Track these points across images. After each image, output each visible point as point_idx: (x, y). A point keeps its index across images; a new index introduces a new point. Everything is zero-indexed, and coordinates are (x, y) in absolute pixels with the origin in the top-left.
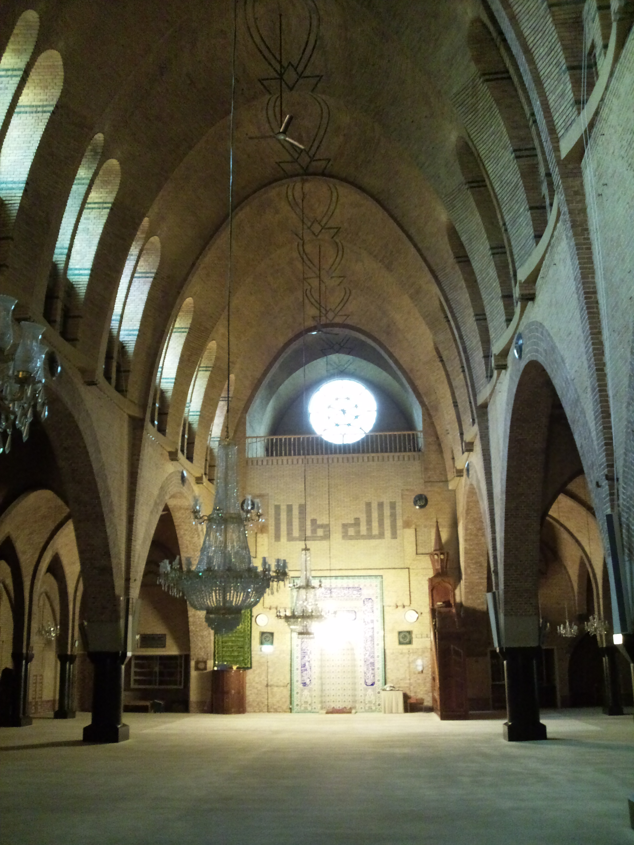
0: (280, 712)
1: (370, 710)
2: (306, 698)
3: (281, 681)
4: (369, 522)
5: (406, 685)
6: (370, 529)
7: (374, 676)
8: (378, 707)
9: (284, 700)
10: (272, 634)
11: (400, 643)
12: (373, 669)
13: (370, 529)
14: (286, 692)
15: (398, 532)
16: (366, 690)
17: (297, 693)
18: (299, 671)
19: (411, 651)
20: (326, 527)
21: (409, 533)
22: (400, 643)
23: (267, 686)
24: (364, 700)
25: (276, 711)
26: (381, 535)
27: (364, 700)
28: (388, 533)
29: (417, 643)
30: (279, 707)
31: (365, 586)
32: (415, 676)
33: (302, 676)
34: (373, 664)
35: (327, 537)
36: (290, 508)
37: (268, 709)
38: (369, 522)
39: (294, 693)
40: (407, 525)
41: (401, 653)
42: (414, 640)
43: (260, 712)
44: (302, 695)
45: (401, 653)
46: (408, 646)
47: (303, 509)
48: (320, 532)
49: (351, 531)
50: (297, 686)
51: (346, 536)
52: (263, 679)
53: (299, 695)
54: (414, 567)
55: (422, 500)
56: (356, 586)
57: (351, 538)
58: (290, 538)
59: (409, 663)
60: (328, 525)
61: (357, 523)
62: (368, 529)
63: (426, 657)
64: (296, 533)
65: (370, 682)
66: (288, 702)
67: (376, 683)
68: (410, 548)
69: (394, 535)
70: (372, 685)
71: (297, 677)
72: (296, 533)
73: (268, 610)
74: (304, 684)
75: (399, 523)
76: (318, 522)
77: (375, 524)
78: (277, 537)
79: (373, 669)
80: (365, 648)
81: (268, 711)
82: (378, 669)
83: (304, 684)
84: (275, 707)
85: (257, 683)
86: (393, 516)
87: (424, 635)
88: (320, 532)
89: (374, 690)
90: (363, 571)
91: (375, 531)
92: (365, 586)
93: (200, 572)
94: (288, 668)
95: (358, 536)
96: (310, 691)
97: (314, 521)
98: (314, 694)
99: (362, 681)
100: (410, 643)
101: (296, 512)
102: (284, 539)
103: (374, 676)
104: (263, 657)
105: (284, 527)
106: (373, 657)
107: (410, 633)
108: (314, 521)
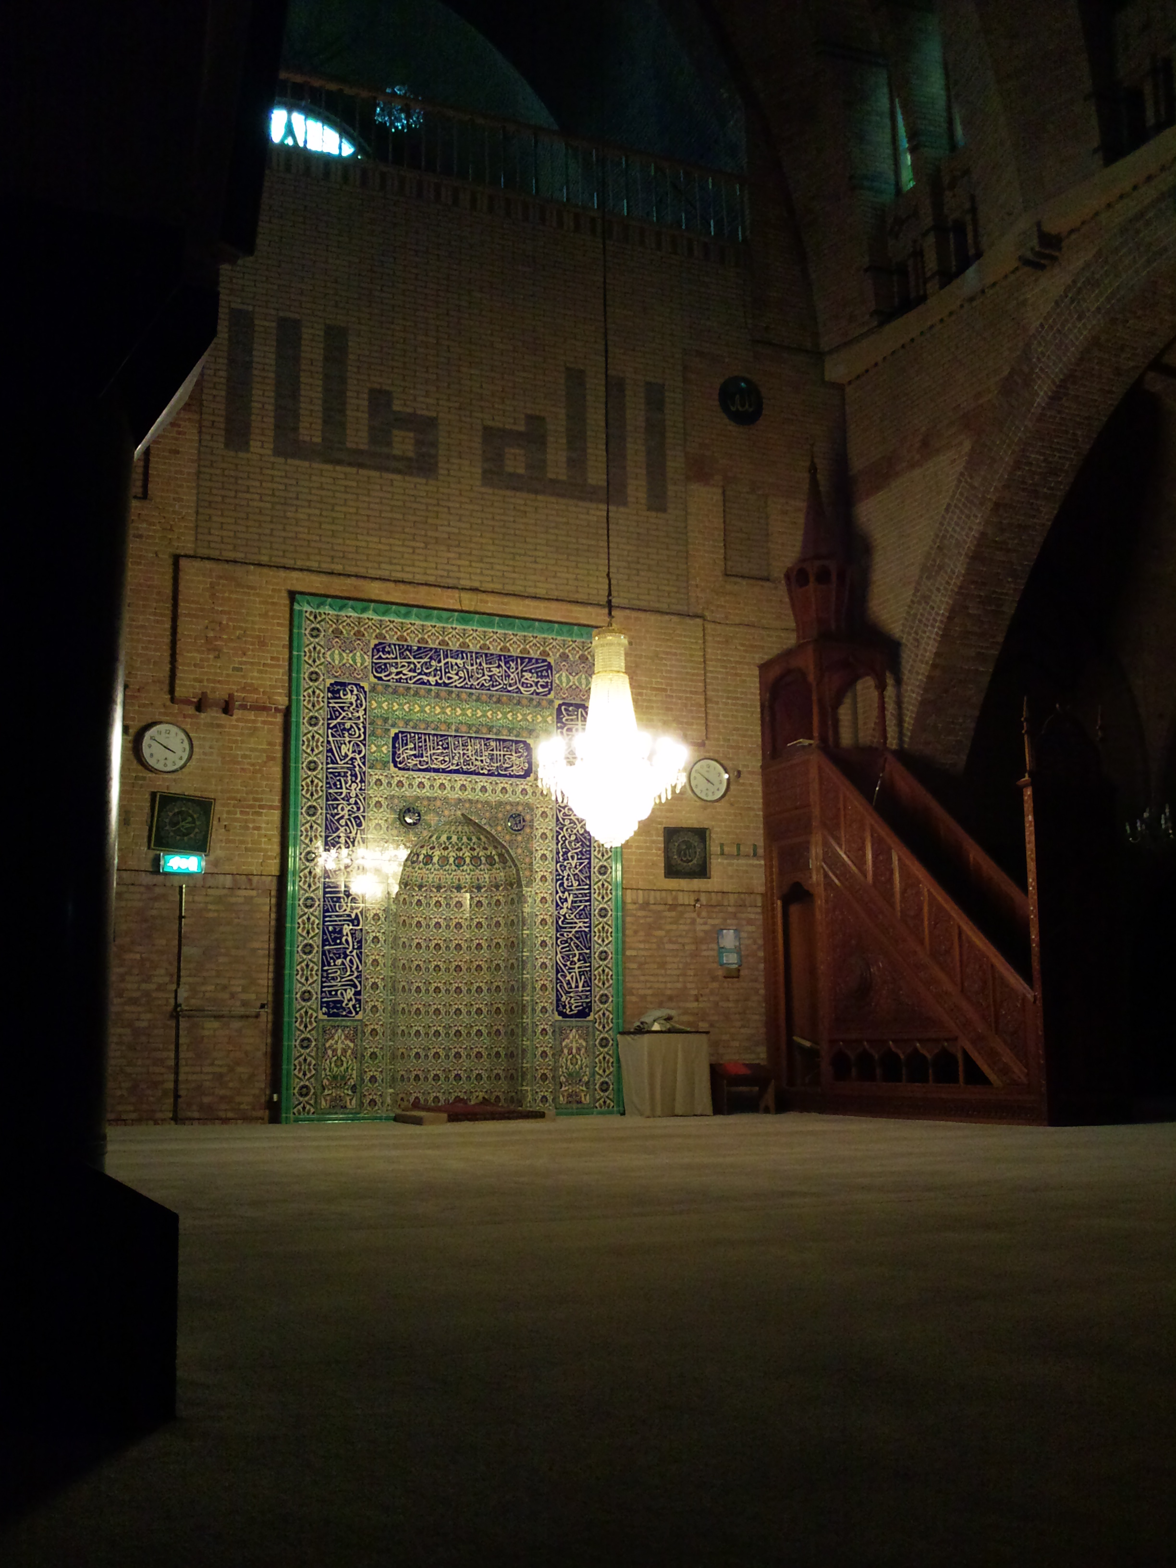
0: (225, 1121)
1: (575, 1107)
2: (339, 1062)
3: (233, 996)
4: (576, 439)
5: (482, 1067)
6: (577, 463)
7: (588, 984)
8: (599, 1094)
9: (243, 1070)
10: (204, 806)
11: (671, 871)
12: (585, 958)
13: (577, 463)
14: (255, 1041)
15: (671, 489)
16: (559, 1033)
17: (305, 1043)
18: (316, 956)
19: (703, 899)
20: (424, 427)
21: (704, 500)
22: (671, 871)
23: (176, 1013)
24: (554, 1069)
25: (210, 1116)
26: (613, 493)
27: (554, 1069)
28: (637, 488)
29: (723, 874)
30: (222, 1098)
31: (564, 657)
32: (715, 985)
33: (326, 977)
34: (584, 938)
35: (423, 465)
36: (289, 334)
37: (175, 1111)
38: (576, 439)
39: (292, 1043)
40: (699, 471)
41: (673, 907)
42: (716, 864)
43: (139, 1121)
44: (322, 1052)
45: (673, 907)
46: (697, 884)
47: (336, 341)
48: (403, 443)
49: (515, 461)
50: (304, 1010)
51: (495, 474)
52: (160, 988)
53: (312, 1050)
54: (719, 616)
55: (742, 403)
56: (534, 654)
57: (514, 483)
58: (288, 444)
59: (698, 942)
60: (431, 423)
61: (534, 435)
62: (571, 463)
63: (750, 922)
64: (311, 430)
65: (573, 1003)
66: (262, 1081)
67: (595, 1007)
68: (706, 554)
69: (658, 501)
70: (583, 1013)
71: (305, 977)
72: (311, 430)
73: (191, 710)
74: (334, 1008)
75: (675, 462)
76: (397, 406)
77: (596, 453)
78: (237, 434)
79: (585, 958)
80: (559, 878)
81: (176, 1119)
82: (604, 956)
83: (334, 1008)
84: (206, 1100)
85: (134, 1001)
86: (655, 430)
87: (746, 849)
88: (403, 443)
89: (587, 1034)
90: (554, 605)
91: (596, 477)
92: (564, 657)
93: (272, 1098)
94: (263, 944)
95: (536, 482)
96: (355, 1034)
97: (379, 400)
98: (370, 1045)
99: (547, 1000)
100: (702, 872)
101: (312, 350)
102: (261, 446)
103: (588, 984)
104: (163, 897)
105: (263, 399)
106: (585, 914)
107: (701, 834)
108: (379, 400)
